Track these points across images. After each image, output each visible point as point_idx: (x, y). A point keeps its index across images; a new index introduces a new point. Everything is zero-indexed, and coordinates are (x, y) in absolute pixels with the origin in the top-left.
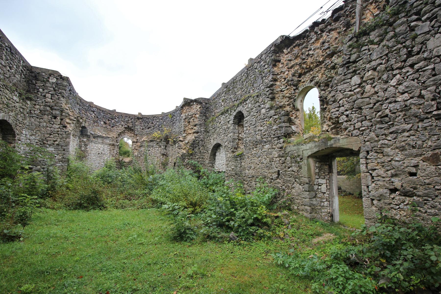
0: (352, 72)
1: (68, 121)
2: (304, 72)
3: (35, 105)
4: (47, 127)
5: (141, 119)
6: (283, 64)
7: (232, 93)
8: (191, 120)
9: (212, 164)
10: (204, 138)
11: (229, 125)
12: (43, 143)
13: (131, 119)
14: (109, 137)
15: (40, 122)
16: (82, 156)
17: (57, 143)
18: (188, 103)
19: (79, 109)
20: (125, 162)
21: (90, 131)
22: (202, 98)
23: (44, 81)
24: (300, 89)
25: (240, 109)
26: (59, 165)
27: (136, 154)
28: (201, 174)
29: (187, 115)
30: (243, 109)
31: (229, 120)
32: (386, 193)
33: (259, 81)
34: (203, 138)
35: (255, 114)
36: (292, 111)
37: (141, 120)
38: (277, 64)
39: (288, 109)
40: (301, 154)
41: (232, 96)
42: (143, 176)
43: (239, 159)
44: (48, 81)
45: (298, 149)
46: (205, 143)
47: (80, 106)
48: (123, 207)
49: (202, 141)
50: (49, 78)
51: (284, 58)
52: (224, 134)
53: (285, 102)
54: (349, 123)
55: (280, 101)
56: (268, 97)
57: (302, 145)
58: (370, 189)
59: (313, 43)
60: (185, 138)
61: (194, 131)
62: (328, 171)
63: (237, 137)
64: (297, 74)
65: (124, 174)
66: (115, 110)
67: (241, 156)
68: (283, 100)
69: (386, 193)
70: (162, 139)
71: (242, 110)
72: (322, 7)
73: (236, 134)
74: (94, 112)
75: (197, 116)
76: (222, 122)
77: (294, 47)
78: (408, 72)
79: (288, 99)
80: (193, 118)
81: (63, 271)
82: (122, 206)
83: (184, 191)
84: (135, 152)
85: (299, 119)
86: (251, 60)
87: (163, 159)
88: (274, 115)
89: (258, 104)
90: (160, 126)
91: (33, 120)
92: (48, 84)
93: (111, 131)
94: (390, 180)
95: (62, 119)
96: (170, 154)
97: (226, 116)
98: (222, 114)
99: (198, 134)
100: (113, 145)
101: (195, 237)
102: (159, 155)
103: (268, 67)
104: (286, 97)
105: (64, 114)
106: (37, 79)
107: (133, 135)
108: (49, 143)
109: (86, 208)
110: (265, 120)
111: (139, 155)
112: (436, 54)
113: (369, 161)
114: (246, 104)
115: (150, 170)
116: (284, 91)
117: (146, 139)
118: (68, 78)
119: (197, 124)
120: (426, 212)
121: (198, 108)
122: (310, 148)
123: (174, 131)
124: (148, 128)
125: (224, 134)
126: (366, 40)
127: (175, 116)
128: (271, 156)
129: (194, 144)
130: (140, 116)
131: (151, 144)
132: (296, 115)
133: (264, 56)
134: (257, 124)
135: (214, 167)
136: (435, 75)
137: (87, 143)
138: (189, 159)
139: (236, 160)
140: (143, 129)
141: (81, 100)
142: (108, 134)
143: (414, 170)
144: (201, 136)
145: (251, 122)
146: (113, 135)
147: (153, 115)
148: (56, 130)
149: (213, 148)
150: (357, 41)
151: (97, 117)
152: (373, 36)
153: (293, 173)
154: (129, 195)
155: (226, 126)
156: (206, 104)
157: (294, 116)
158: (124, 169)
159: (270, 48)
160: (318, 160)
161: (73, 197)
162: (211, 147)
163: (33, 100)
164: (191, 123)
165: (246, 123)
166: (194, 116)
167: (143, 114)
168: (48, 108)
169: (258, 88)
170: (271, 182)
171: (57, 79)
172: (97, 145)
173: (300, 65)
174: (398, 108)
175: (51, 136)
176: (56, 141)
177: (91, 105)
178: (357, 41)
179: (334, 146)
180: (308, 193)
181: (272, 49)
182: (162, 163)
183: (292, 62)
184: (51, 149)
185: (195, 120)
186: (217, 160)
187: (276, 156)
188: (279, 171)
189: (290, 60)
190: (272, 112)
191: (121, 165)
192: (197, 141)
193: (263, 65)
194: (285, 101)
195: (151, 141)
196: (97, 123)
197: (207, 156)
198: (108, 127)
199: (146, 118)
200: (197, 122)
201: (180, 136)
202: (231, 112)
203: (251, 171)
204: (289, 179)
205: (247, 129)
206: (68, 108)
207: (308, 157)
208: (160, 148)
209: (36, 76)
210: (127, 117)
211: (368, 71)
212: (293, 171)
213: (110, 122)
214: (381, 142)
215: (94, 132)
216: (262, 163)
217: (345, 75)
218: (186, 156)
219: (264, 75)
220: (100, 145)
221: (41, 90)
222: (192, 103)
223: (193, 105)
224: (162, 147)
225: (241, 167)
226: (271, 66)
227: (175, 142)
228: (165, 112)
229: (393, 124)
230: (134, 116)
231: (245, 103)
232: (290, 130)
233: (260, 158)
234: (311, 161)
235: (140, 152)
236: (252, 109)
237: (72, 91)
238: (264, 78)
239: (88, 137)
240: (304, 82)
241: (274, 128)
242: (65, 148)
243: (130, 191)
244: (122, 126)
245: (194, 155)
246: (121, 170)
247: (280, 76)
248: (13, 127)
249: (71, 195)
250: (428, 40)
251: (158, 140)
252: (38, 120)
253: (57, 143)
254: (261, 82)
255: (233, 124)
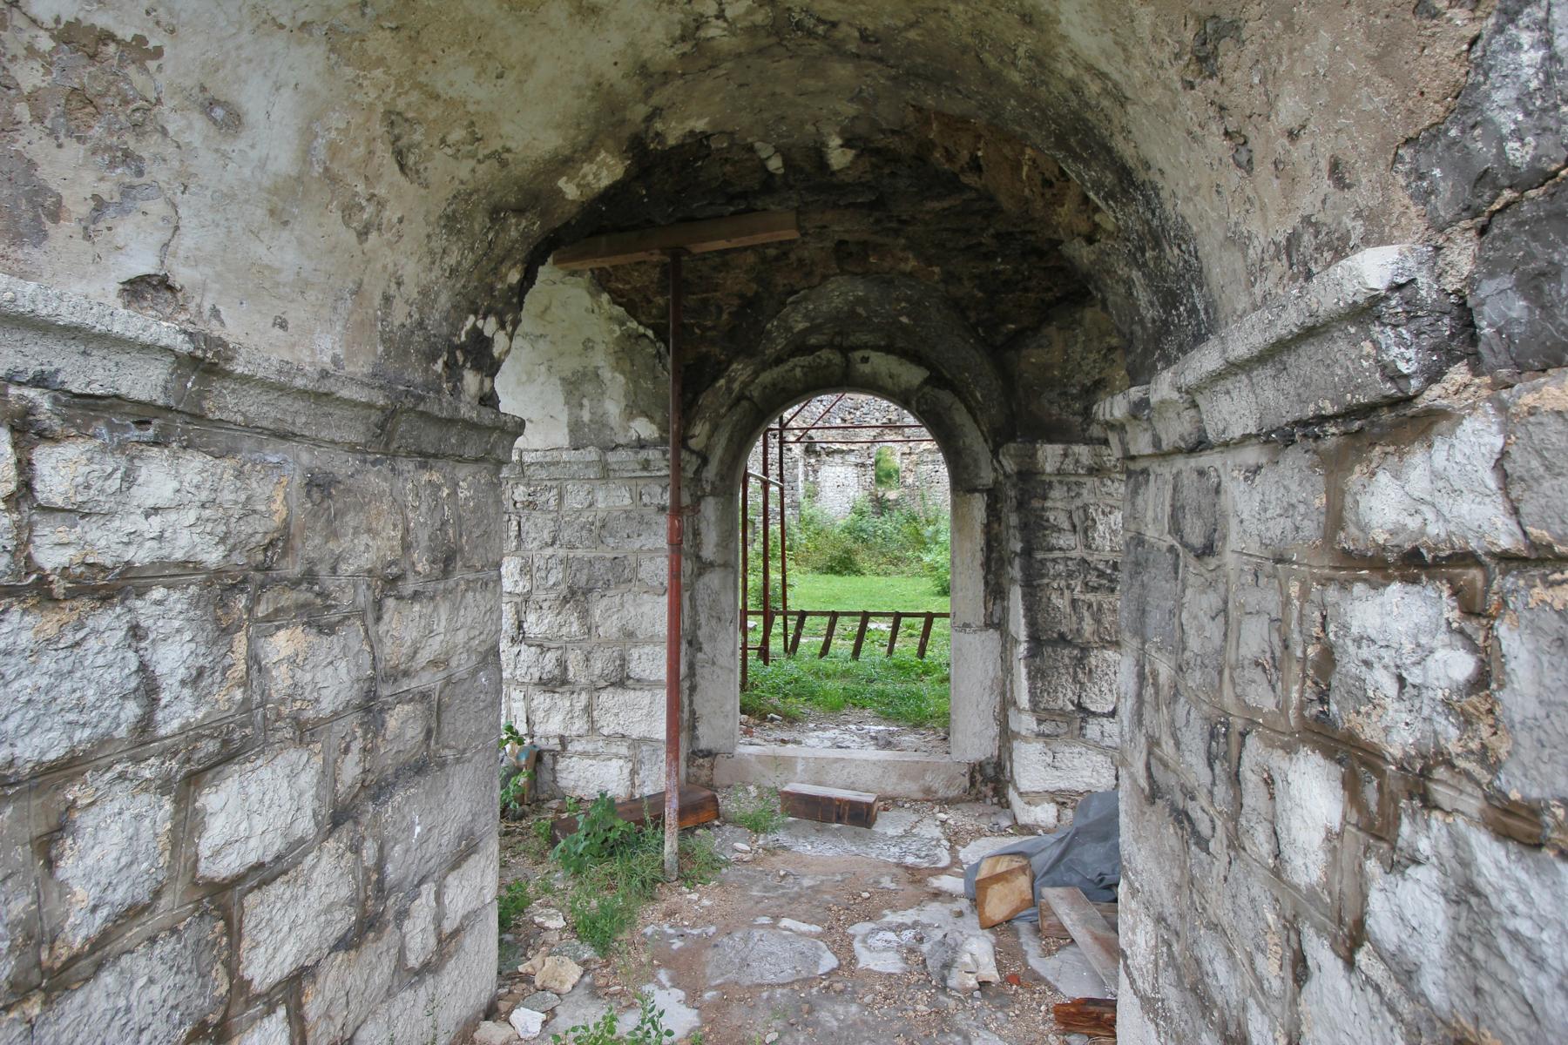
16: (812, 495)
81: (355, 831)
83: (527, 680)
100: (863, 465)
109: (839, 573)
191: (881, 506)
220: (839, 469)
239: (818, 454)
249: (815, 557)
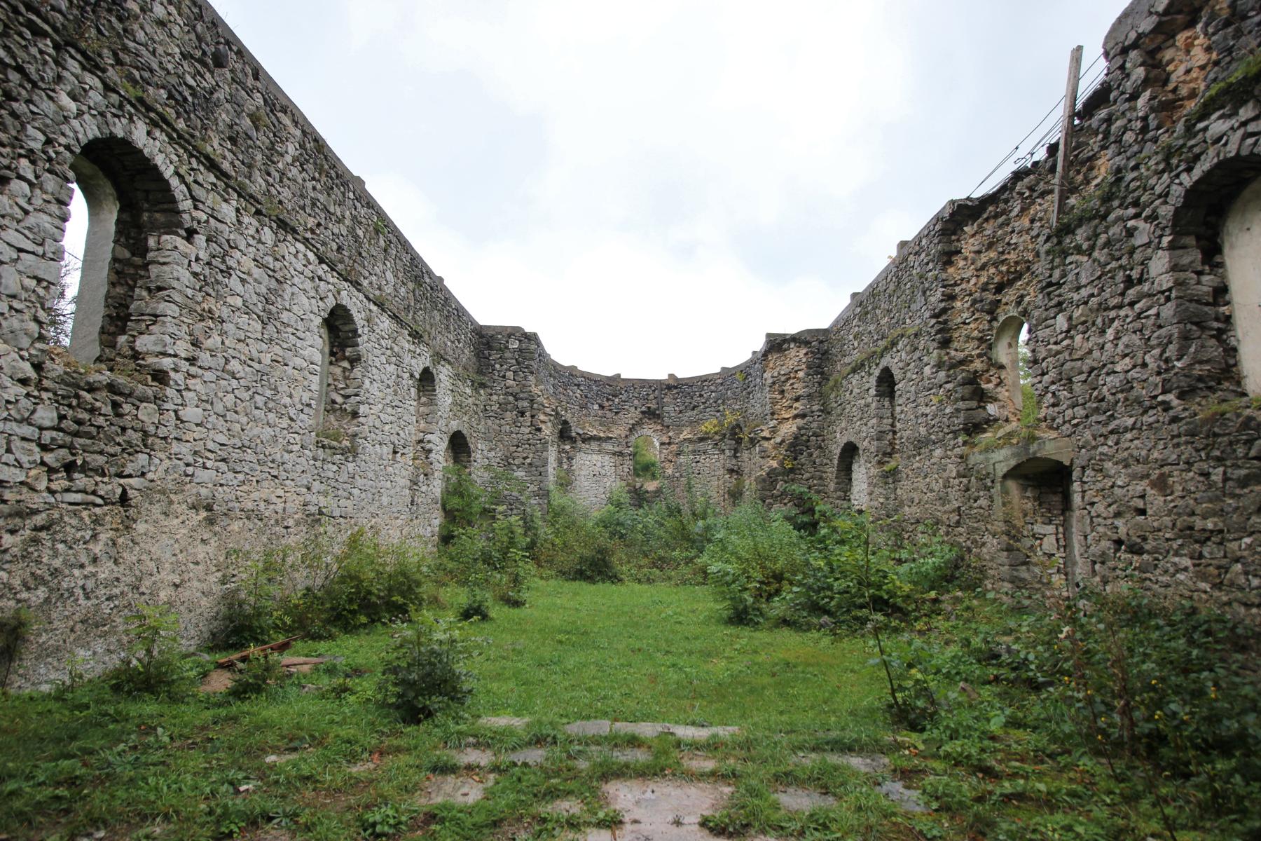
0: (1056, 306)
1: (542, 417)
2: (1008, 280)
3: (491, 395)
4: (512, 432)
5: (676, 387)
6: (966, 259)
7: (872, 319)
8: (787, 387)
9: (845, 492)
10: (821, 428)
11: (870, 400)
12: (507, 462)
13: (654, 391)
14: (611, 438)
15: (500, 426)
16: (566, 483)
17: (528, 461)
18: (777, 344)
19: (553, 386)
20: (647, 492)
21: (575, 430)
22: (809, 331)
23: (500, 349)
24: (1001, 319)
25: (884, 362)
26: (535, 502)
27: (670, 471)
28: (816, 516)
29: (776, 374)
30: (892, 361)
31: (867, 386)
32: (1109, 548)
33: (920, 299)
34: (819, 427)
35: (914, 376)
36: (987, 371)
37: (675, 391)
38: (954, 259)
39: (978, 365)
40: (992, 471)
41: (872, 328)
42: (685, 522)
43: (890, 480)
44: (507, 348)
45: (987, 460)
46: (823, 441)
47: (555, 378)
48: (649, 581)
49: (815, 434)
50: (507, 342)
51: (969, 244)
52: (861, 419)
53: (973, 349)
54: (1056, 409)
55: (963, 347)
56: (934, 340)
57: (993, 451)
58: (1089, 541)
59: (1017, 216)
60: (774, 430)
61: (796, 412)
62: (1061, 507)
63: (889, 427)
64: (992, 286)
65: (649, 518)
66: (619, 375)
67: (894, 473)
68: (967, 345)
69: (1109, 548)
70: (724, 435)
71: (889, 365)
72: (1017, 148)
73: (885, 421)
74: (578, 385)
75: (801, 374)
76: (856, 391)
77: (987, 220)
78: (1127, 316)
79: (976, 342)
80: (791, 381)
82: (648, 579)
84: (667, 466)
85: (1006, 388)
86: (903, 244)
87: (731, 481)
88: (947, 382)
89: (918, 354)
90: (720, 401)
91: (490, 422)
92: (508, 355)
93: (614, 423)
94: (1113, 524)
95: (533, 417)
96: (746, 471)
97: (863, 377)
98: (854, 371)
99: (805, 421)
100: (621, 454)
101: (761, 620)
102: (722, 471)
103: (934, 268)
104: (973, 338)
105: (535, 406)
106: (490, 348)
107: (659, 427)
108: (516, 462)
109: (590, 579)
110: (932, 391)
111: (677, 475)
112: (1159, 289)
113: (1086, 487)
114: (898, 351)
115: (699, 511)
116: (969, 323)
117: (690, 436)
118: (535, 334)
119: (800, 396)
120: (1157, 582)
121: (802, 356)
122: (1006, 459)
123: (750, 411)
124: (693, 409)
125: (861, 419)
126: (1071, 243)
127: (750, 374)
128: (945, 475)
129: (797, 445)
130: (672, 382)
131: (701, 446)
132: (999, 378)
133: (924, 242)
134: (919, 401)
135: (849, 500)
136: (1160, 327)
137: (571, 454)
138: (786, 482)
139: (886, 483)
140: (681, 412)
141: (555, 365)
142: (609, 430)
143: (1140, 504)
144: (814, 425)
145: (908, 396)
146: (619, 431)
147: (700, 377)
148: (526, 437)
149: (841, 454)
150: (1059, 243)
151: (586, 397)
152: (1081, 235)
153: (982, 511)
154: (660, 559)
155: (863, 401)
156: (821, 342)
157: (995, 381)
158: (646, 508)
159: (935, 225)
160: (1031, 483)
161: (568, 561)
162: (838, 451)
163: (488, 387)
164: (786, 394)
165: (900, 395)
166: (792, 375)
167: (679, 376)
168: (511, 398)
169: (918, 314)
170: (947, 534)
171: (520, 341)
172: (590, 457)
173: (996, 264)
174: (1118, 385)
175: (520, 449)
176: (527, 457)
177: (572, 372)
178: (1059, 243)
179: (1038, 455)
180: (1005, 553)
181: (938, 227)
182: (729, 492)
183: (982, 255)
184: (520, 474)
185: (795, 386)
186: (854, 483)
187: (954, 474)
188: (959, 507)
189: (979, 252)
190: (942, 374)
191: (639, 498)
192: (805, 438)
193: (925, 261)
194: (972, 349)
195: (701, 440)
196: (586, 408)
197: (831, 471)
198: (609, 414)
199: (686, 384)
200: (800, 389)
201: (763, 427)
202: (870, 367)
203: (914, 509)
204: (975, 525)
205: (902, 412)
206: (540, 393)
207: (1005, 477)
208: (722, 456)
209: (488, 343)
210: (644, 387)
211: (1078, 306)
212: (981, 508)
213: (611, 403)
214: (1100, 449)
215: (583, 429)
216: (932, 491)
217: (1046, 310)
218: (779, 474)
219: (927, 285)
221: (497, 366)
222: (785, 346)
223: (789, 349)
224: (727, 452)
225: (896, 499)
226: (939, 267)
227: (753, 442)
228: (731, 365)
229: (1112, 415)
230: (660, 382)
231: (894, 349)
232: (979, 415)
233: (928, 480)
234: (1012, 485)
235: (678, 467)
236: (908, 365)
237: (543, 355)
238: (928, 293)
240: (1007, 304)
241: (948, 411)
242: (541, 469)
243: (661, 552)
244: (636, 408)
245: (798, 472)
246: (641, 511)
247: (960, 288)
248: (468, 436)
249: (561, 557)
250: (1150, 259)
251: (717, 437)
252: (498, 422)
253: (528, 461)
254: (923, 302)
255: (876, 396)
